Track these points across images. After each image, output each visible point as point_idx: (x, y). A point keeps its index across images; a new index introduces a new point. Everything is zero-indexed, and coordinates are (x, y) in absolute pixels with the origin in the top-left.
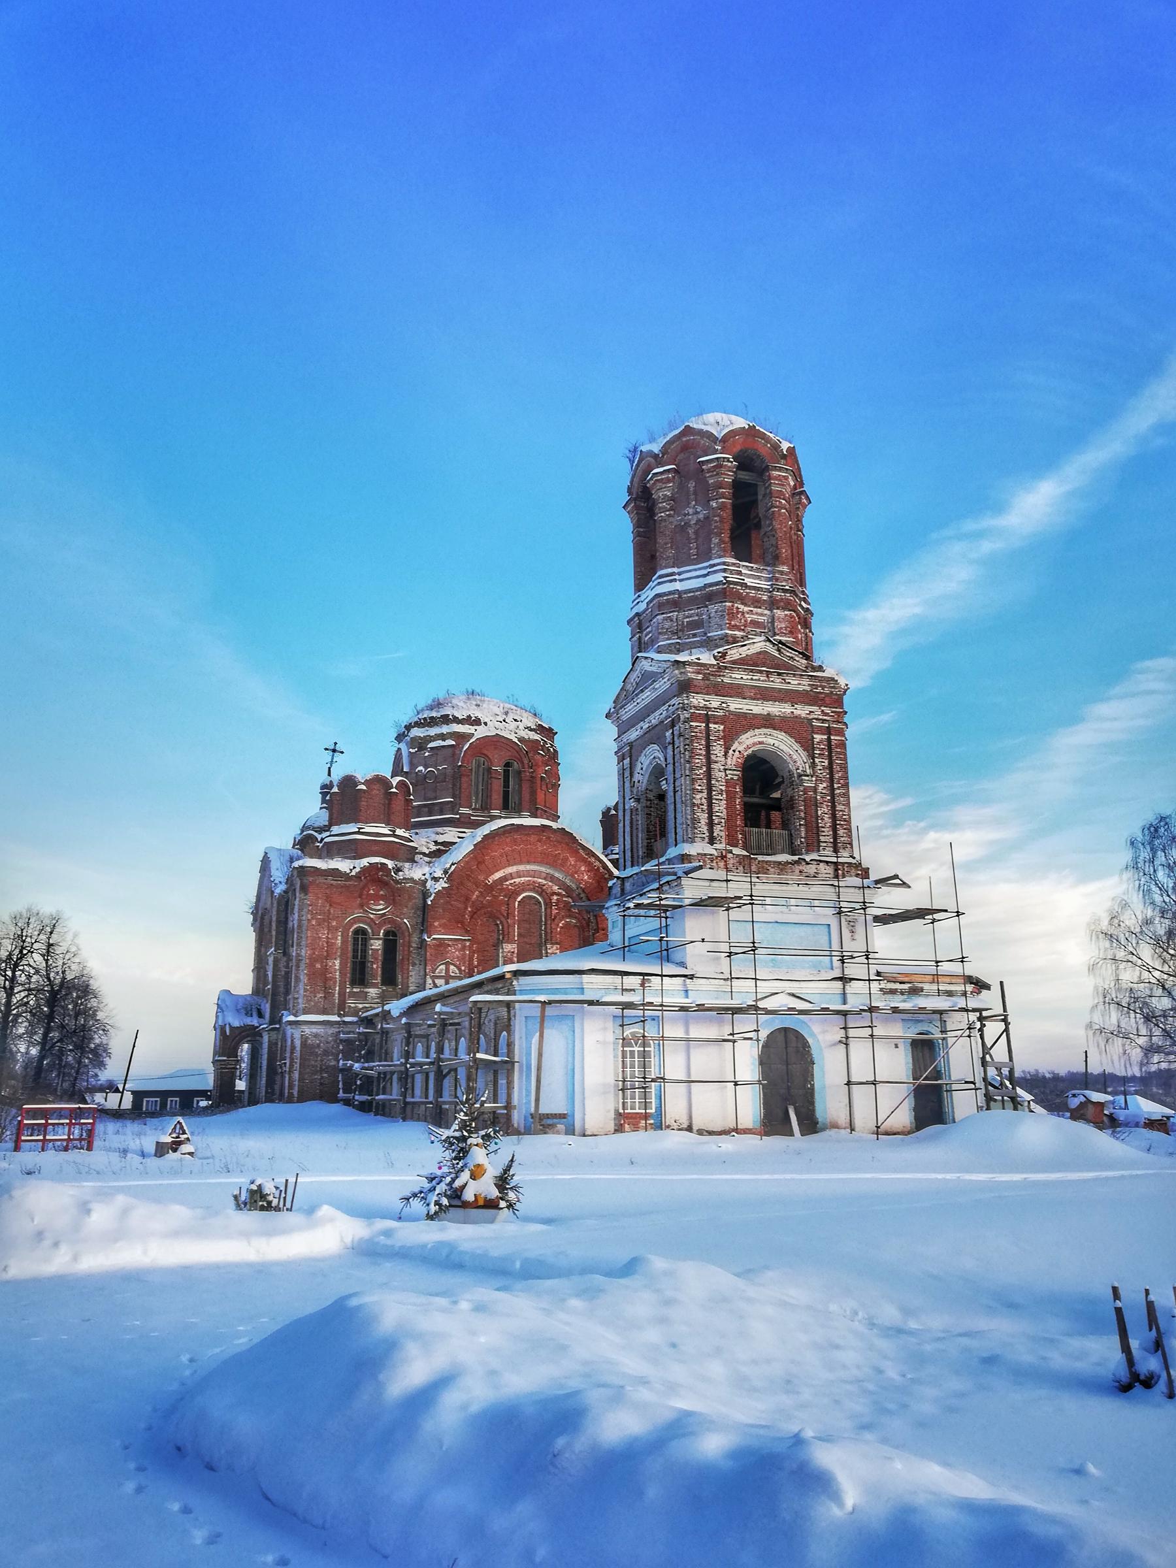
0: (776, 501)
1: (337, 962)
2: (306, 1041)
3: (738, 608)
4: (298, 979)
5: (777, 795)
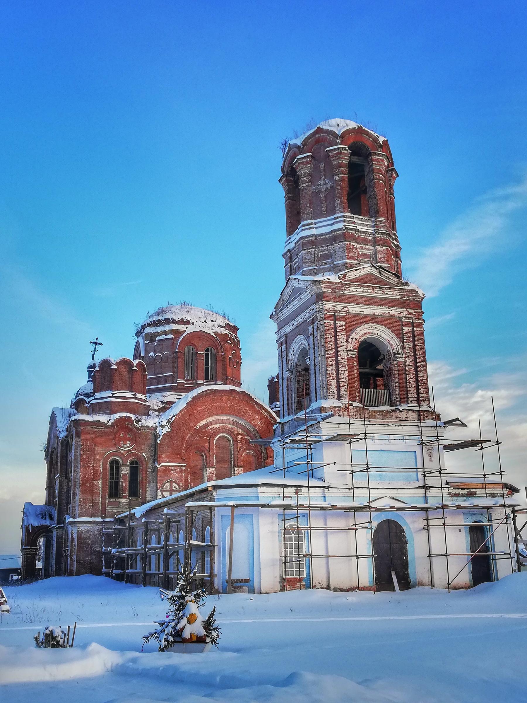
1: (100, 482)
2: (81, 535)
4: (75, 494)
5: (380, 367)
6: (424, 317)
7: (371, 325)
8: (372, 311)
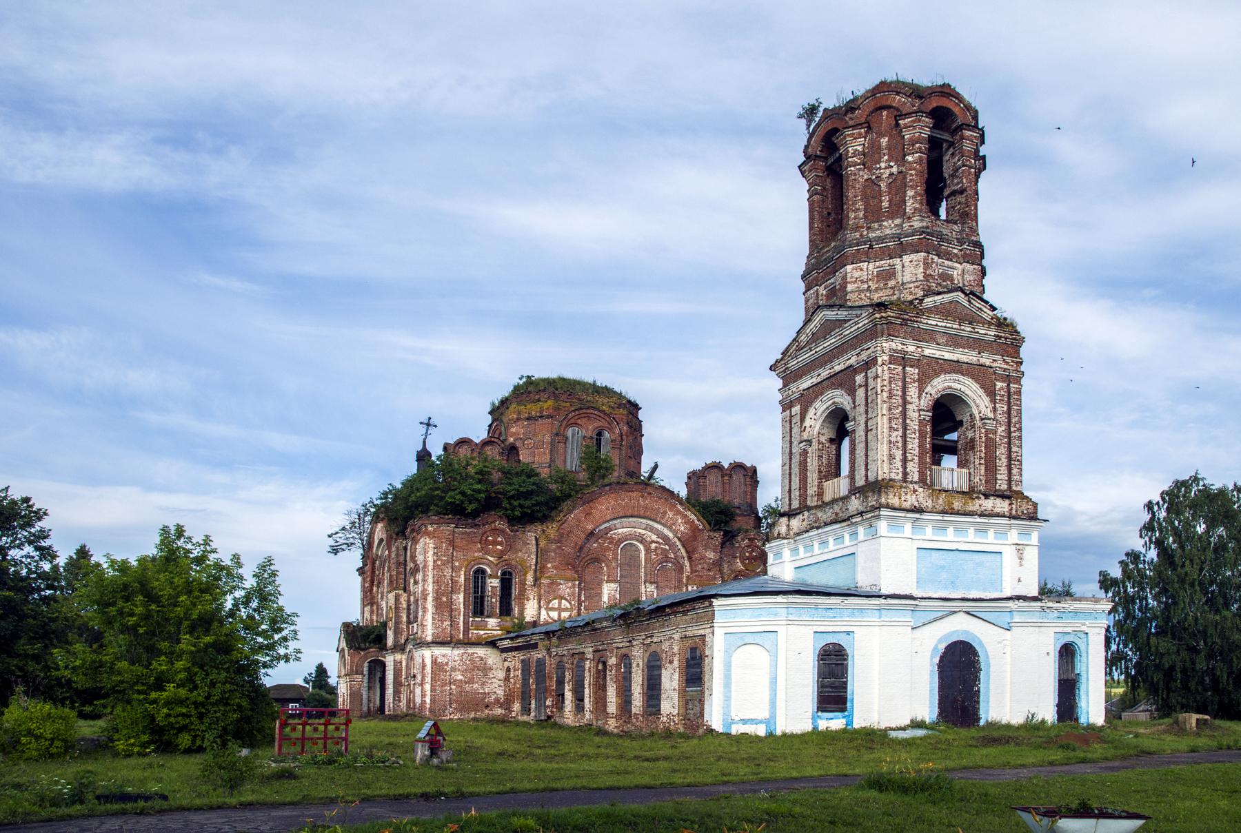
0: (967, 160)
1: (461, 596)
2: (436, 660)
3: (932, 259)
4: (425, 609)
5: (953, 436)
6: (1023, 368)
7: (955, 376)
8: (956, 355)
